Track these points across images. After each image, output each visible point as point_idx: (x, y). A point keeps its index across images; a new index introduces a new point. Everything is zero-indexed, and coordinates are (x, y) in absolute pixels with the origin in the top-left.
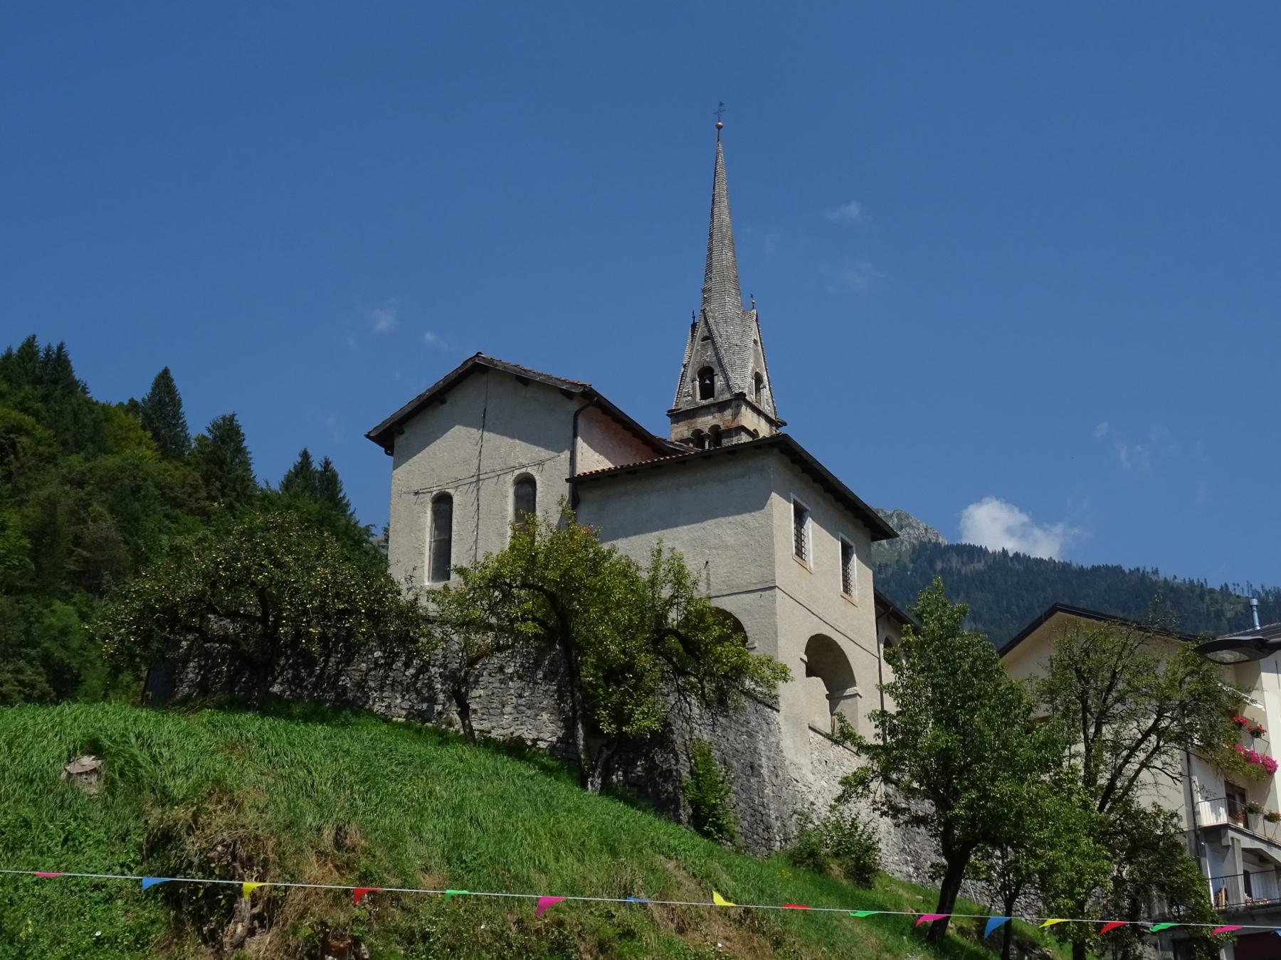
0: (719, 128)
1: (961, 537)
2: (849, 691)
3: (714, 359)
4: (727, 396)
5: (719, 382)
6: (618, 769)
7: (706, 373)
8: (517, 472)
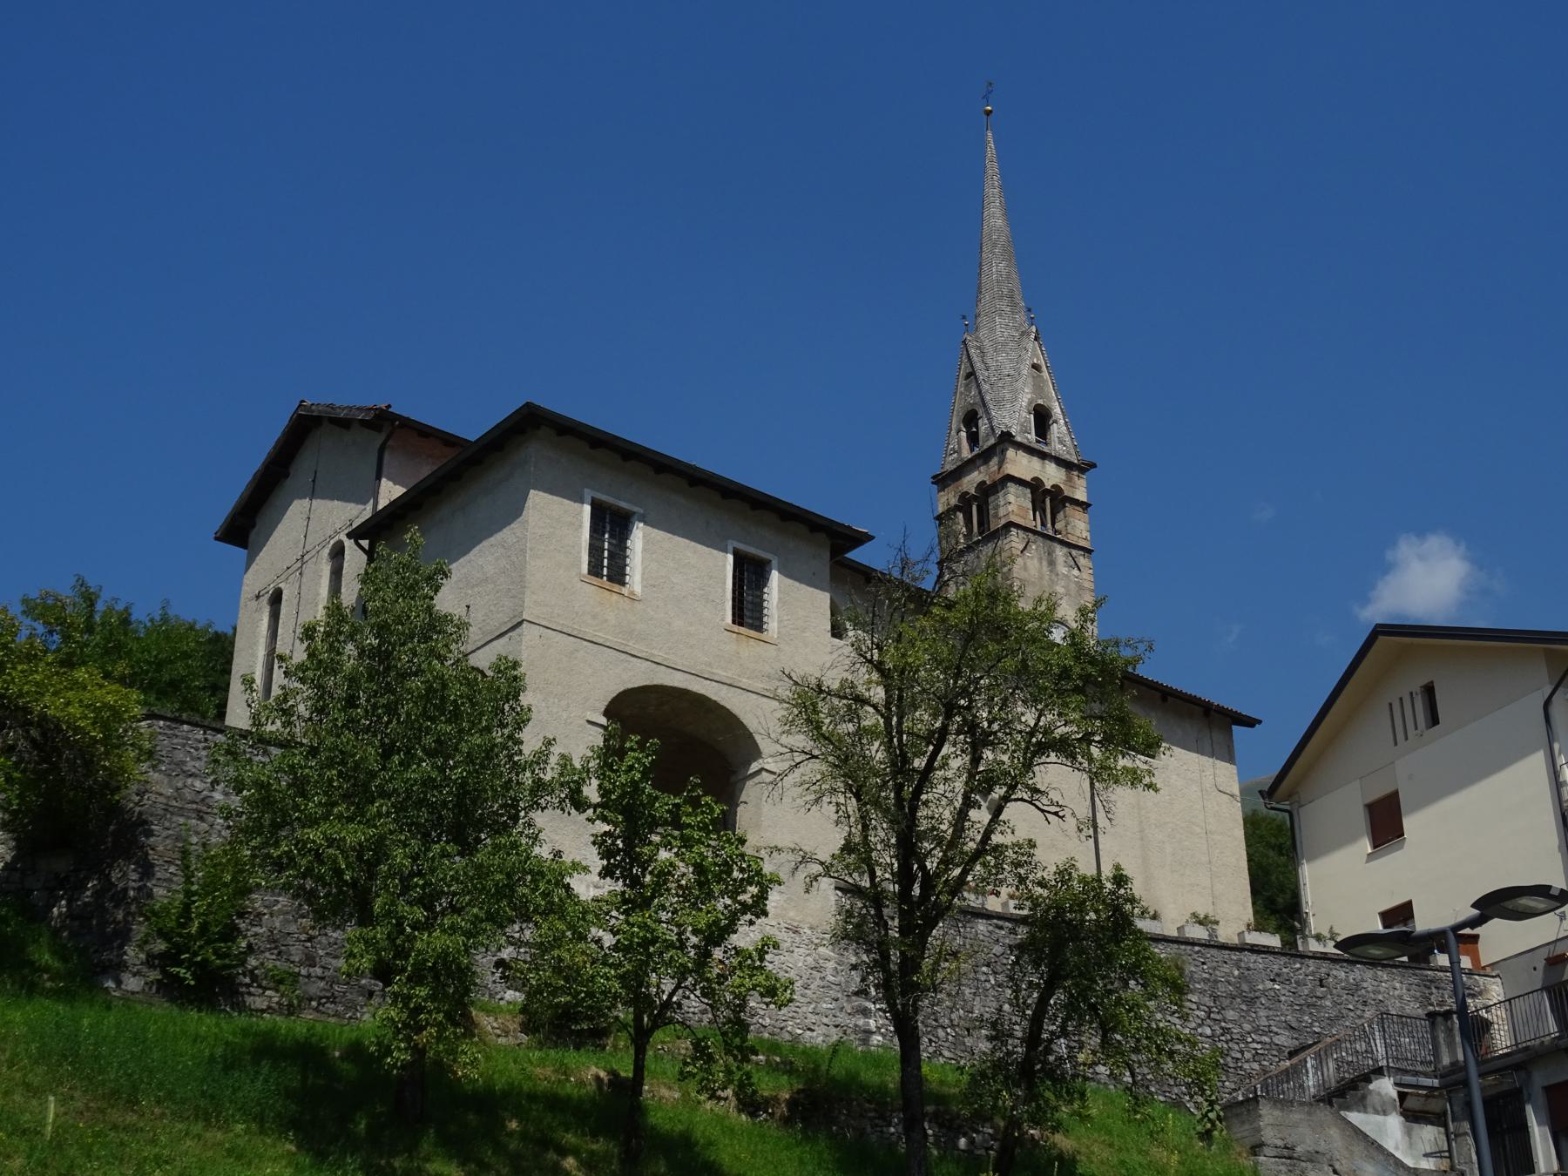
0: (988, 113)
1: (389, 479)
2: (754, 767)
3: (978, 399)
4: (992, 441)
5: (983, 426)
6: (62, 898)
7: (971, 419)
8: (327, 551)
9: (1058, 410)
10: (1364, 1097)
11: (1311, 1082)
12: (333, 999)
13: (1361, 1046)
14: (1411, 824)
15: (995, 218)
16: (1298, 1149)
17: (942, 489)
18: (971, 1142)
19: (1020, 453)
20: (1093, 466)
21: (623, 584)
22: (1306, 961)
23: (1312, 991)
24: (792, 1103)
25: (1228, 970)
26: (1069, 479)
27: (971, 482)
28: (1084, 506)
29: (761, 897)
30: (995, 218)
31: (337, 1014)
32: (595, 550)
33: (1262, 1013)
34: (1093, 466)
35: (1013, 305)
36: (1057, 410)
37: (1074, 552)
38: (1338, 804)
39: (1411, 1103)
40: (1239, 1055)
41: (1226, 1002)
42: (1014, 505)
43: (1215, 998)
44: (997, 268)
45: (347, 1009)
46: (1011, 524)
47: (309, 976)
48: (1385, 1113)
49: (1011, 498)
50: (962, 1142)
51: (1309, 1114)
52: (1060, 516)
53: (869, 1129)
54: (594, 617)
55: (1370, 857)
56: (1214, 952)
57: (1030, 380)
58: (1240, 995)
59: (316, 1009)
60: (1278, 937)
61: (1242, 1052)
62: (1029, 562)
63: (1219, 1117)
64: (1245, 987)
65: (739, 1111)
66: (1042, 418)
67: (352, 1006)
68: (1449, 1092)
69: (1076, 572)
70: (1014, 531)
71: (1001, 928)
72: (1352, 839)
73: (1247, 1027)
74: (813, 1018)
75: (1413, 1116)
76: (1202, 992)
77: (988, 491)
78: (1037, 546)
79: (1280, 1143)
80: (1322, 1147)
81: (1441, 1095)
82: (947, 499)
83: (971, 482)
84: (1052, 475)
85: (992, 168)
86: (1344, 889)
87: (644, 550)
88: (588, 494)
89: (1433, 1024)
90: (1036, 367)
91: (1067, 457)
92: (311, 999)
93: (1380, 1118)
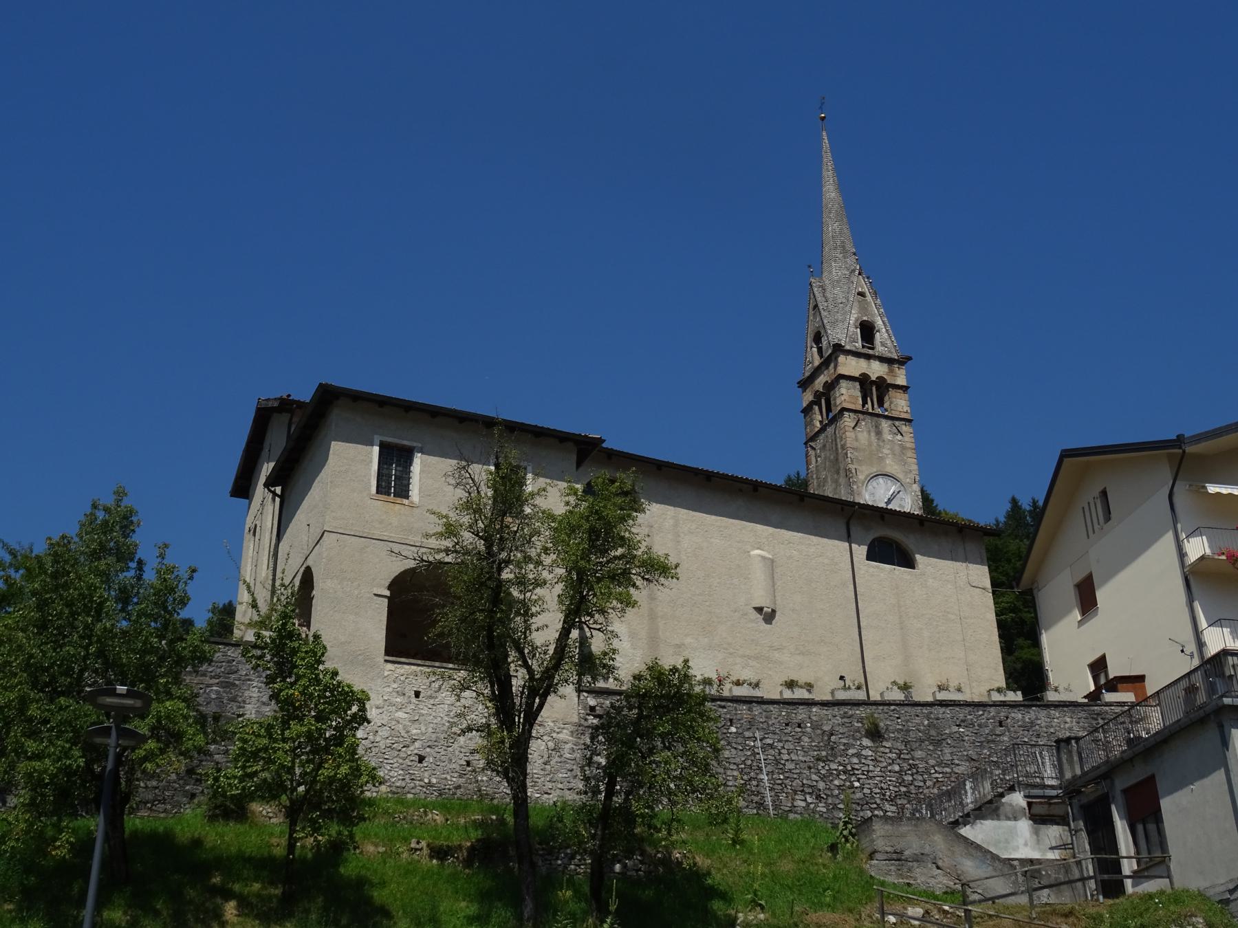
0: (823, 119)
9: (880, 322)
10: (997, 808)
11: (969, 799)
12: (164, 801)
13: (1031, 769)
14: (1101, 595)
15: (830, 192)
16: (906, 853)
17: (804, 391)
18: (625, 866)
19: (850, 357)
20: (910, 359)
21: (407, 497)
22: (988, 709)
23: (992, 730)
24: (472, 849)
25: (919, 721)
26: (891, 371)
27: (819, 383)
28: (904, 389)
29: (363, 709)
30: (830, 192)
31: (165, 811)
32: (382, 476)
33: (947, 751)
34: (910, 359)
35: (844, 251)
36: (879, 322)
37: (897, 423)
38: (1056, 590)
39: (1037, 810)
40: (921, 784)
41: (915, 745)
42: (847, 395)
43: (906, 743)
44: (834, 227)
45: (174, 807)
46: (844, 409)
47: (146, 787)
48: (1015, 819)
49: (843, 391)
50: (618, 867)
51: (916, 825)
52: (886, 398)
53: (540, 863)
54: (381, 522)
55: (1080, 623)
56: (906, 709)
57: (856, 304)
58: (928, 739)
59: (150, 809)
60: (1019, 693)
61: (925, 781)
62: (860, 435)
63: (850, 833)
64: (933, 732)
65: (431, 857)
66: (867, 331)
67: (178, 805)
68: (1070, 798)
69: (899, 437)
70: (846, 414)
71: (724, 707)
72: (1068, 611)
73: (932, 762)
74: (550, 785)
75: (1039, 819)
76: (896, 739)
77: (831, 386)
78: (866, 423)
79: (889, 849)
80: (927, 850)
81: (1063, 802)
82: (808, 397)
83: (819, 383)
84: (876, 370)
85: (827, 158)
86: (1067, 652)
87: (422, 471)
88: (377, 439)
89: (1058, 749)
90: (861, 294)
91: (889, 355)
92: (146, 803)
93: (1009, 823)
